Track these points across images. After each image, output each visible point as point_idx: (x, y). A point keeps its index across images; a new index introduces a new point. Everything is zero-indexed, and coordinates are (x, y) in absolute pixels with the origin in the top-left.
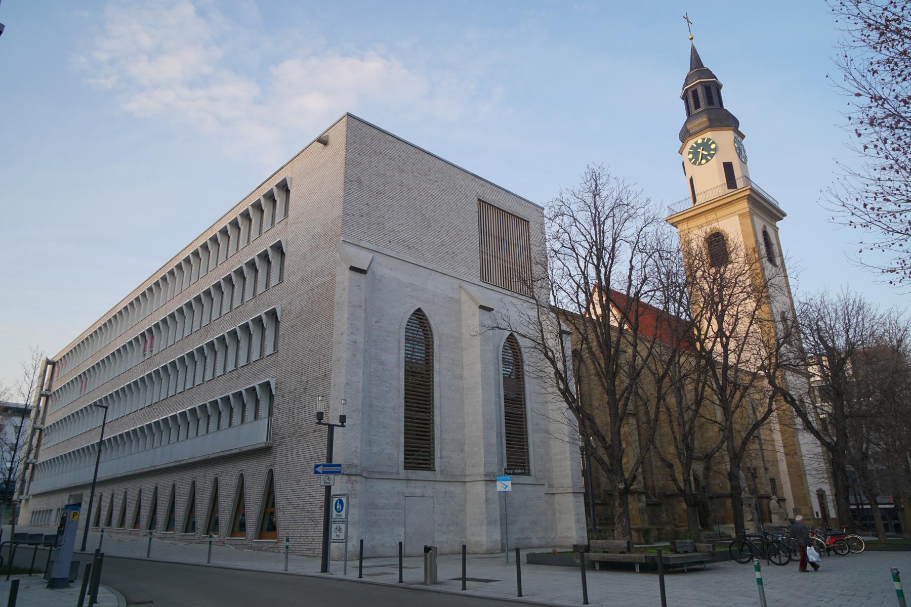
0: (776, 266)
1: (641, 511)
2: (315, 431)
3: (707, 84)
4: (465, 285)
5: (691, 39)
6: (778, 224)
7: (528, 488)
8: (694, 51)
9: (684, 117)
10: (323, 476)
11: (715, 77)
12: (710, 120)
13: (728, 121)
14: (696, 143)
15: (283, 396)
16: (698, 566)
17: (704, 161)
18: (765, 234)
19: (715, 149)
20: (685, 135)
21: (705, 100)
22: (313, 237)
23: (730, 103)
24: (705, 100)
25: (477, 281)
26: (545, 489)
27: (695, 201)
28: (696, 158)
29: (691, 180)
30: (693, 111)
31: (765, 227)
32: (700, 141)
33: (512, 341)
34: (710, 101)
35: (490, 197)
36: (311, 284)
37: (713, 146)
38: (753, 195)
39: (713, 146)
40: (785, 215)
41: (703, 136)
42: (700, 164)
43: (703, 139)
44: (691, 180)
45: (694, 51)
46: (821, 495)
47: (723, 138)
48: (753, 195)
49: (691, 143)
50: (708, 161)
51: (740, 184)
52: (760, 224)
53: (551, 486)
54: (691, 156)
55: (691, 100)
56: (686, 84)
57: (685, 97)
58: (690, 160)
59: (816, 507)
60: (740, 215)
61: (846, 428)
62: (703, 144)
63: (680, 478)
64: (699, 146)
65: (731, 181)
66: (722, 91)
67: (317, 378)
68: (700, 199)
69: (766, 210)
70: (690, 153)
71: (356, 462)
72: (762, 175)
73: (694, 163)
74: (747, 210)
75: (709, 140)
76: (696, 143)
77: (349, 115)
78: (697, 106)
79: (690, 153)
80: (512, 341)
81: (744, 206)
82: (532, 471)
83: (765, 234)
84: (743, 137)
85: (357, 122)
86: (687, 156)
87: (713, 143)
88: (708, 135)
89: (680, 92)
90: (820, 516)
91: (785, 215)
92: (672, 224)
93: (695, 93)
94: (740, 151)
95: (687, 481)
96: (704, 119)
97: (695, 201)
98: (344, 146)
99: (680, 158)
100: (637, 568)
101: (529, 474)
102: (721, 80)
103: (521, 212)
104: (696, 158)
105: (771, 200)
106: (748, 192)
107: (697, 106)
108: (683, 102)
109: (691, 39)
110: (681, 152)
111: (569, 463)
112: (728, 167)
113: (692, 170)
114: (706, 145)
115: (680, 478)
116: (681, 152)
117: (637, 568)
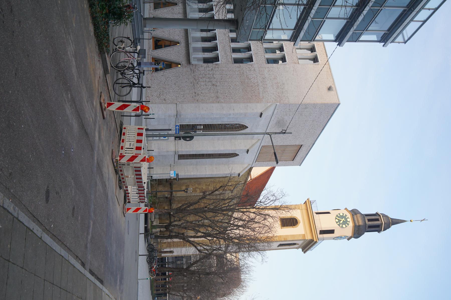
0: (278, 246)
1: (164, 195)
2: (195, 93)
3: (381, 227)
4: (260, 141)
5: (411, 221)
6: (300, 250)
7: (173, 159)
9: (363, 213)
10: (175, 128)
12: (359, 226)
13: (358, 232)
14: (348, 218)
15: (212, 69)
17: (337, 220)
18: (295, 244)
19: (342, 227)
20: (354, 212)
21: (372, 224)
22: (284, 84)
23: (367, 235)
24: (372, 224)
25: (262, 144)
26: (173, 164)
27: (317, 213)
28: (339, 217)
29: (329, 213)
30: (367, 218)
31: (298, 244)
32: (348, 220)
34: (370, 227)
35: (303, 150)
36: (261, 85)
37: (344, 226)
38: (313, 242)
39: (344, 226)
40: (304, 253)
41: (351, 222)
42: (336, 219)
43: (349, 222)
44: (329, 213)
46: (171, 252)
47: (349, 230)
48: (313, 242)
49: (349, 215)
50: (337, 222)
51: (320, 236)
52: (300, 243)
53: (174, 166)
54: (341, 214)
56: (384, 216)
57: (377, 214)
58: (339, 214)
59: (165, 250)
60: (304, 235)
62: (347, 221)
63: (176, 223)
64: (346, 219)
65: (323, 232)
66: (377, 232)
67: (217, 92)
68: (316, 216)
69: (307, 245)
70: (343, 214)
71: (182, 117)
72: (325, 246)
73: (337, 216)
74: (306, 239)
75: (348, 224)
76: (348, 218)
77: (339, 104)
78: (369, 220)
79: (343, 214)
81: (309, 237)
82: (180, 161)
83: (295, 244)
84: (348, 239)
85: (332, 113)
86: (343, 212)
87: (346, 226)
88: (351, 224)
89: (379, 212)
91: (304, 253)
92: (306, 202)
93: (377, 220)
94: (340, 238)
95: (174, 226)
96: (361, 223)
97: (317, 213)
98: (326, 102)
99: (343, 208)
100: (146, 226)
101: (179, 159)
102: (382, 233)
103: (298, 158)
104: (339, 217)
105: (314, 246)
106: (315, 240)
107: (369, 220)
108: (374, 213)
109: (411, 221)
110: (346, 209)
111: (183, 174)
112: (332, 232)
113: (334, 214)
114: (346, 222)
115: (176, 223)
116: (346, 209)
117: (146, 226)
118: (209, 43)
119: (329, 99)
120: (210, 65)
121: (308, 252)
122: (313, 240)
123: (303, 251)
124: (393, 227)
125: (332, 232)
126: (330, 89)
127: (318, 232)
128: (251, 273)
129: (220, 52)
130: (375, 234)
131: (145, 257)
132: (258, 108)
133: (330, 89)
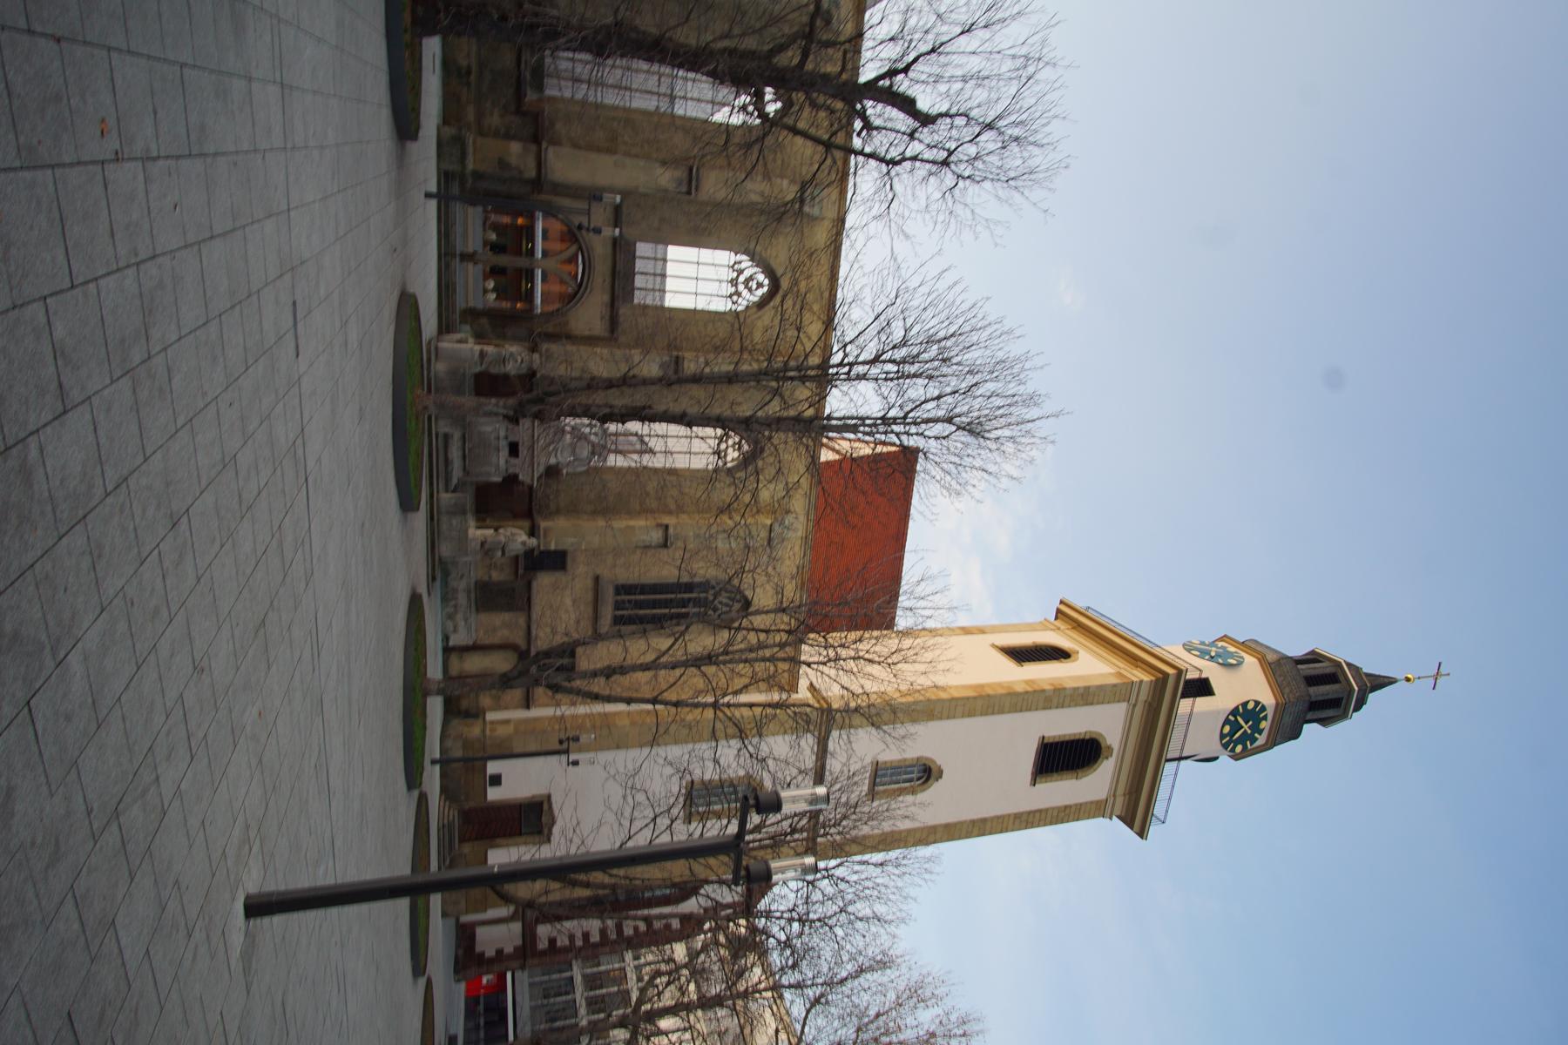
8: (1389, 681)
11: (1361, 703)
21: (1320, 691)
24: (1320, 691)
40: (1142, 833)
45: (1389, 681)
72: (1200, 790)
90: (494, 794)
91: (1142, 833)
92: (1058, 611)
102: (1356, 722)
109: (1408, 680)
121: (1154, 830)
122: (1166, 675)
123: (1130, 825)
124: (1372, 697)
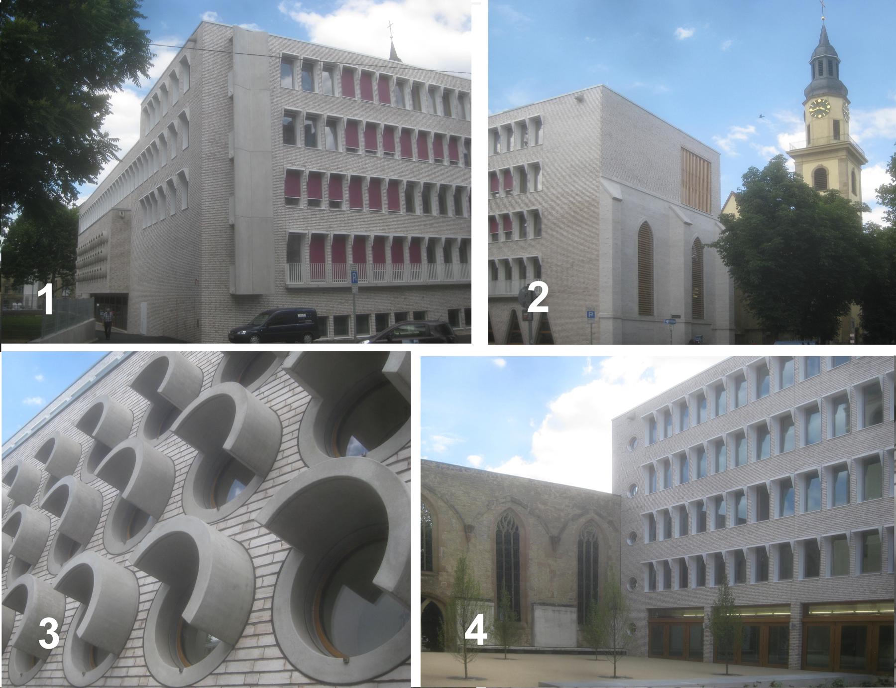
13: (838, 90)
16: (504, 583)
23: (844, 77)
25: (679, 203)
33: (645, 233)
34: (831, 72)
35: (689, 146)
37: (828, 107)
47: (834, 103)
52: (851, 166)
55: (817, 68)
57: (812, 64)
61: (58, 631)
80: (645, 233)
84: (849, 102)
89: (809, 59)
93: (821, 64)
102: (840, 57)
103: (706, 156)
107: (821, 73)
108: (810, 67)
110: (804, 104)
112: (836, 124)
118: (513, 269)
119: (594, 99)
120: (543, 270)
121: (867, 157)
125: (836, 124)
126: (580, 100)
127: (837, 141)
128: (886, 215)
129: (525, 255)
130: (842, 67)
131: (730, 666)
132: (606, 209)
133: (580, 100)
